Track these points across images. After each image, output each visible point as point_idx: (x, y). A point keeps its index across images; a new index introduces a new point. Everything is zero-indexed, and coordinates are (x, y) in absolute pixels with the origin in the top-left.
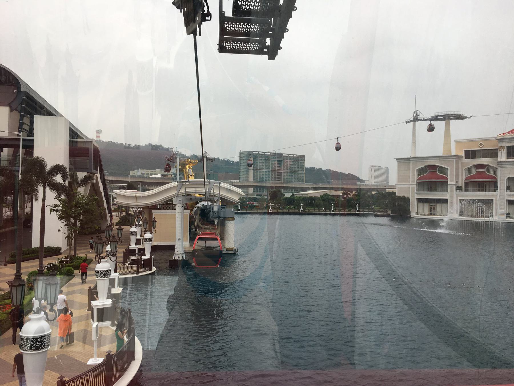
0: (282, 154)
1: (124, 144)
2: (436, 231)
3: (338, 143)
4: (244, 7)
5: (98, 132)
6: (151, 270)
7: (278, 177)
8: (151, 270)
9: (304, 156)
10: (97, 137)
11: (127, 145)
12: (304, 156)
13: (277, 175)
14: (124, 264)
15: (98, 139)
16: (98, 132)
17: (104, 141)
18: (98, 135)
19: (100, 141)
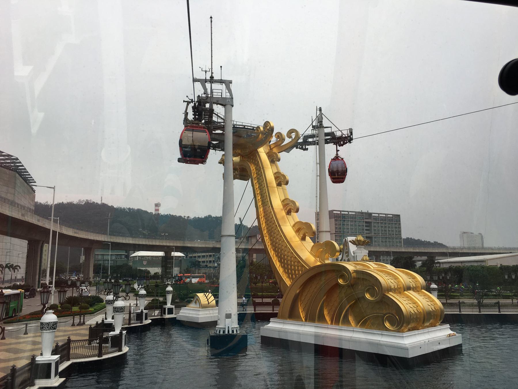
0: (371, 214)
1: (183, 216)
2: (229, 345)
3: (337, 158)
5: (157, 205)
6: (120, 350)
8: (120, 350)
9: (399, 216)
11: (186, 218)
12: (399, 216)
13: (366, 226)
14: (90, 344)
15: (157, 212)
16: (157, 205)
18: (157, 208)
19: (159, 214)
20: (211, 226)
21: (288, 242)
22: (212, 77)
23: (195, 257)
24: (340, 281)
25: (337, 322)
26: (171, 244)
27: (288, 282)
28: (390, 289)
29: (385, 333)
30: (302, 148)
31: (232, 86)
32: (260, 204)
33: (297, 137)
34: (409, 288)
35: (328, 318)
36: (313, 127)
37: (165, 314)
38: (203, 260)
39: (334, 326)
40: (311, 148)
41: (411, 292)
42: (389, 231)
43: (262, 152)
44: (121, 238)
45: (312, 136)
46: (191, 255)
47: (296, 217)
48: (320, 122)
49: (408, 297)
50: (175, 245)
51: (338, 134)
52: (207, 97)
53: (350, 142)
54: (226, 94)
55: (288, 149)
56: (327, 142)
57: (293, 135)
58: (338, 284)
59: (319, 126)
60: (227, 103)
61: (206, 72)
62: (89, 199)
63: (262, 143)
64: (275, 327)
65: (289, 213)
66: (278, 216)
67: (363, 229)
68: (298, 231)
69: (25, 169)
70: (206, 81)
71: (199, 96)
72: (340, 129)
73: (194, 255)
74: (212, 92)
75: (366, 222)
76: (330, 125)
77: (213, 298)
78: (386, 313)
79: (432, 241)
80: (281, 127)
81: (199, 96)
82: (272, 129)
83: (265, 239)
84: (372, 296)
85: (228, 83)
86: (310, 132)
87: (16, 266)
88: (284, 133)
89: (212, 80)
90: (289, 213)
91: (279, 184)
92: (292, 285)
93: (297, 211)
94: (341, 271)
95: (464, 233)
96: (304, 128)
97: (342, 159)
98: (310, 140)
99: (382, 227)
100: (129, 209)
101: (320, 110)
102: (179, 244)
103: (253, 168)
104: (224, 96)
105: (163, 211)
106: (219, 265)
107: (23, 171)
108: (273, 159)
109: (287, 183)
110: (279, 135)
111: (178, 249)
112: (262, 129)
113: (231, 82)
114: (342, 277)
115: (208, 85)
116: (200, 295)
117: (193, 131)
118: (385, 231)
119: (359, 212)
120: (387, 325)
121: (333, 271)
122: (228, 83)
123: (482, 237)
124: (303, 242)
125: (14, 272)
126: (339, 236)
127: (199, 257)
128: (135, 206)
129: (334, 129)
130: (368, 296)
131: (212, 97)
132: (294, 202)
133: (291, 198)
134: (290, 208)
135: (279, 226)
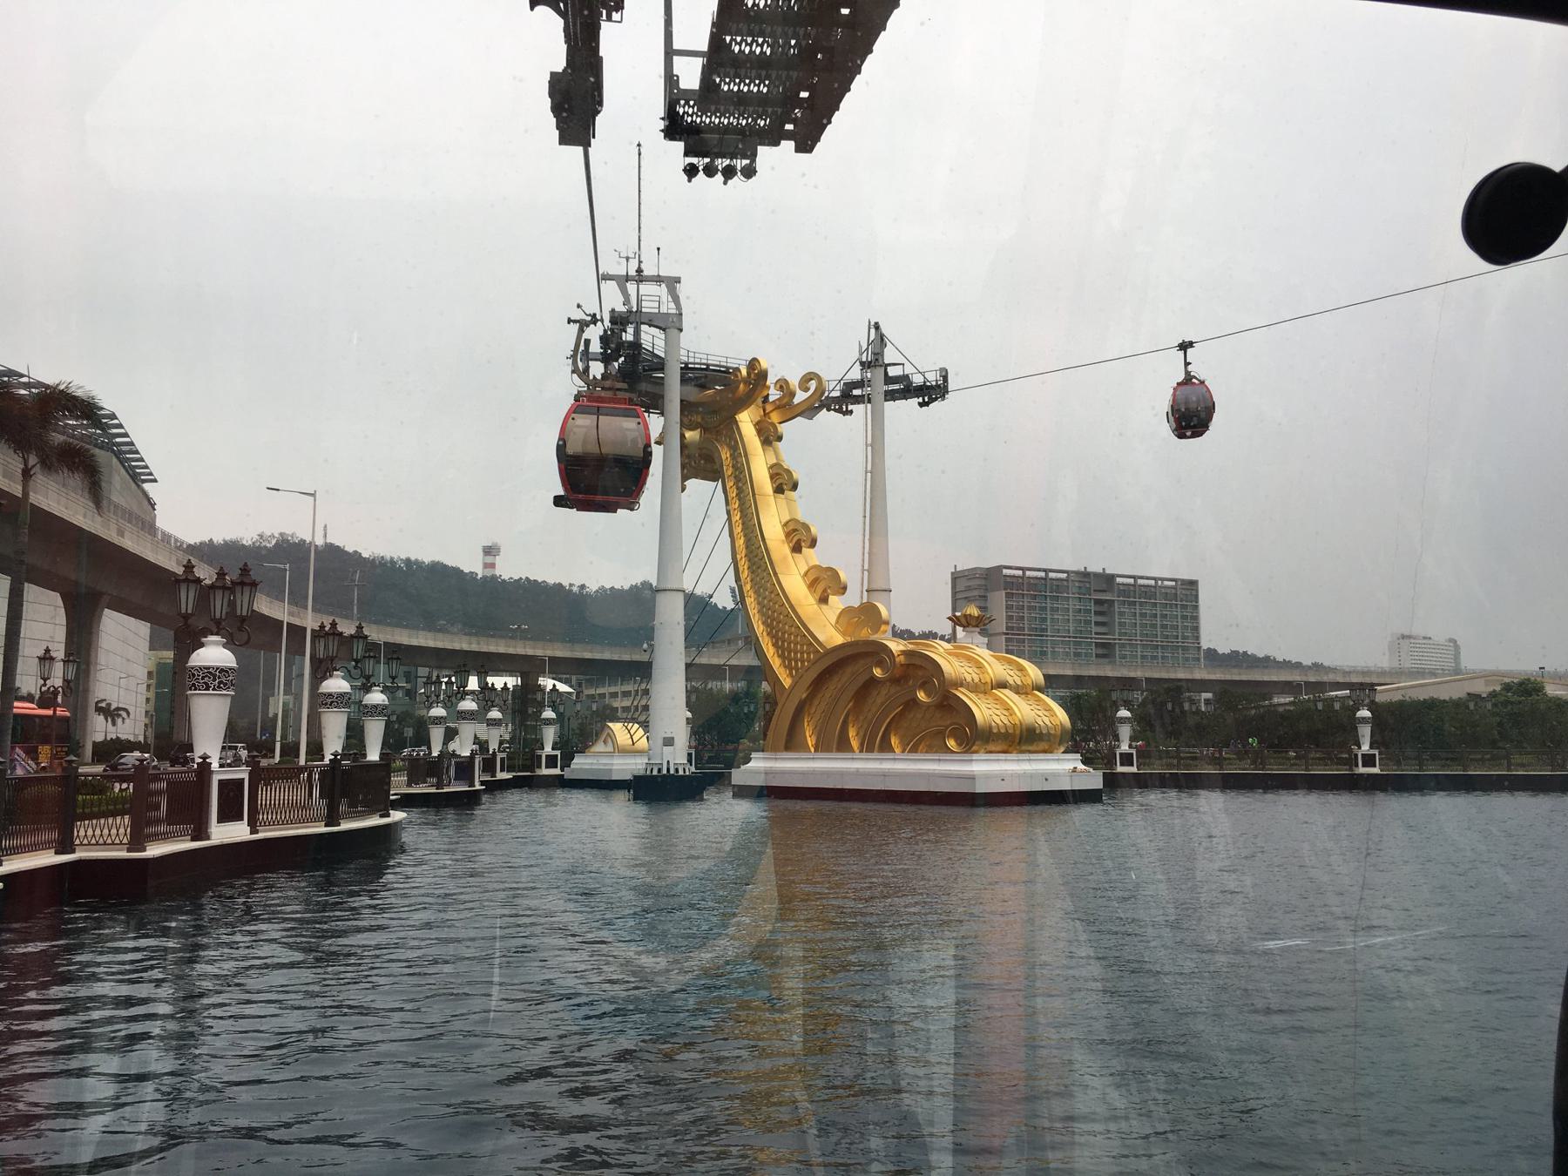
0: (1112, 577)
1: (566, 584)
3: (1188, 379)
4: (737, 49)
5: (490, 551)
7: (1100, 619)
10: (486, 566)
11: (575, 589)
15: (489, 573)
16: (490, 551)
17: (505, 577)
18: (489, 559)
19: (494, 577)
20: (642, 599)
21: (792, 606)
22: (639, 271)
23: (603, 696)
24: (877, 672)
25: (870, 749)
26: (539, 653)
27: (787, 682)
28: (960, 683)
29: (948, 757)
30: (839, 411)
31: (682, 290)
32: (738, 529)
33: (820, 390)
34: (1003, 685)
35: (855, 744)
36: (862, 364)
37: (540, 767)
38: (627, 703)
39: (864, 755)
40: (858, 409)
41: (1006, 691)
42: (1163, 626)
43: (746, 421)
44: (405, 632)
45: (860, 384)
46: (592, 692)
47: (812, 557)
48: (878, 355)
49: (997, 699)
50: (549, 653)
51: (917, 380)
52: (630, 311)
53: (943, 397)
54: (668, 307)
55: (809, 411)
56: (891, 396)
57: (813, 385)
58: (873, 679)
59: (874, 361)
60: (670, 324)
61: (627, 259)
62: (289, 532)
63: (743, 404)
64: (759, 766)
65: (797, 549)
66: (774, 558)
67: (1088, 622)
68: (812, 585)
69: (132, 444)
70: (627, 278)
71: (613, 311)
72: (922, 370)
73: (600, 691)
74: (639, 301)
75: (1098, 602)
76: (901, 359)
77: (641, 732)
78: (948, 719)
79: (1307, 662)
80: (783, 367)
81: (613, 311)
82: (763, 375)
83: (748, 601)
84: (928, 695)
85: (672, 283)
86: (855, 374)
87: (118, 709)
88: (794, 382)
89: (640, 277)
90: (797, 549)
91: (779, 490)
92: (793, 687)
93: (813, 543)
94: (877, 652)
95: (1403, 637)
96: (839, 367)
97: (1202, 382)
98: (857, 392)
99: (1143, 615)
100: (408, 561)
101: (877, 327)
102: (560, 652)
103: (725, 454)
104: (664, 310)
105: (509, 569)
106: (651, 646)
107: (124, 448)
108: (769, 437)
109: (795, 487)
110: (783, 385)
111: (558, 667)
112: (744, 372)
113: (678, 280)
114: (880, 664)
115: (631, 287)
116: (616, 727)
117: (598, 412)
118: (1154, 626)
119: (1077, 573)
120: (951, 743)
121: (866, 655)
122: (672, 283)
123: (1457, 647)
124: (824, 607)
125: (114, 724)
126: (1018, 641)
127: (614, 695)
128: (426, 554)
129: (909, 370)
130: (921, 695)
131: (639, 311)
132: (807, 527)
133: (801, 517)
134: (800, 539)
135: (775, 574)
